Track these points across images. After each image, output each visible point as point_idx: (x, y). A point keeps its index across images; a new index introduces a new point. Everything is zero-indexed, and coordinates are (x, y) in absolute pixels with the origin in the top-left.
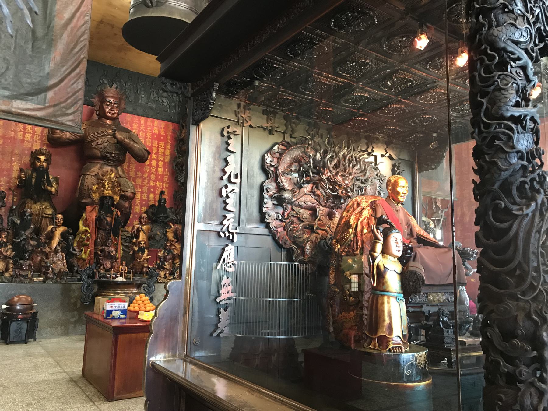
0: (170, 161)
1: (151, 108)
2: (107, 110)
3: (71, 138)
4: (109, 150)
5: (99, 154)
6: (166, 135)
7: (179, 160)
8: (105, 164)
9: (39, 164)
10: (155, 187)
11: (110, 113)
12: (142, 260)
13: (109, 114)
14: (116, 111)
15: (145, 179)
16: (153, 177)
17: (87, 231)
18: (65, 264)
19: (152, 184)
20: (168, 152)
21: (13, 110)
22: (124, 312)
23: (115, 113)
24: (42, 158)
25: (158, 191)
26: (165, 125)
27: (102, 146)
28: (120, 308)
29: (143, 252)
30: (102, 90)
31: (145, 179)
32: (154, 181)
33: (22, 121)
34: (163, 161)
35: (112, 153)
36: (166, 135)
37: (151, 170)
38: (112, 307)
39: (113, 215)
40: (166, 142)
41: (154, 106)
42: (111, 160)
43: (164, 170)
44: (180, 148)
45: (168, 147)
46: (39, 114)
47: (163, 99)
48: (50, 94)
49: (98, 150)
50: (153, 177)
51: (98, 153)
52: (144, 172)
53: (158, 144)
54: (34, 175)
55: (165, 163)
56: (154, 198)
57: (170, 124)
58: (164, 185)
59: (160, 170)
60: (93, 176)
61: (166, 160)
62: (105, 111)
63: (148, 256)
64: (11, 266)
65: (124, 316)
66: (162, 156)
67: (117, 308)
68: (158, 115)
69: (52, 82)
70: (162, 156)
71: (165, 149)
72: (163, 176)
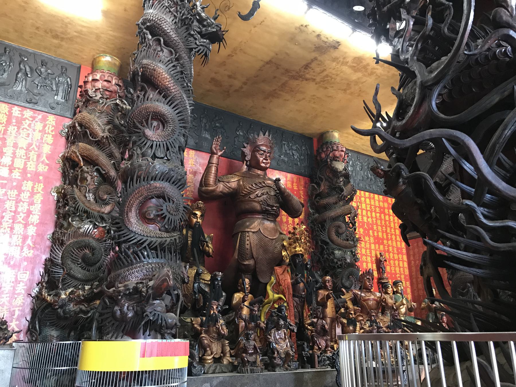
1: (283, 161)
2: (261, 159)
3: (224, 191)
6: (299, 190)
9: (195, 220)
11: (264, 163)
13: (263, 165)
14: (269, 161)
17: (280, 298)
18: (288, 344)
23: (268, 163)
24: (198, 213)
26: (297, 179)
27: (261, 198)
30: (254, 138)
35: (273, 206)
36: (299, 190)
41: (286, 159)
47: (294, 152)
51: (257, 206)
54: (190, 233)
57: (302, 178)
60: (253, 232)
62: (259, 161)
64: (228, 349)
68: (290, 168)
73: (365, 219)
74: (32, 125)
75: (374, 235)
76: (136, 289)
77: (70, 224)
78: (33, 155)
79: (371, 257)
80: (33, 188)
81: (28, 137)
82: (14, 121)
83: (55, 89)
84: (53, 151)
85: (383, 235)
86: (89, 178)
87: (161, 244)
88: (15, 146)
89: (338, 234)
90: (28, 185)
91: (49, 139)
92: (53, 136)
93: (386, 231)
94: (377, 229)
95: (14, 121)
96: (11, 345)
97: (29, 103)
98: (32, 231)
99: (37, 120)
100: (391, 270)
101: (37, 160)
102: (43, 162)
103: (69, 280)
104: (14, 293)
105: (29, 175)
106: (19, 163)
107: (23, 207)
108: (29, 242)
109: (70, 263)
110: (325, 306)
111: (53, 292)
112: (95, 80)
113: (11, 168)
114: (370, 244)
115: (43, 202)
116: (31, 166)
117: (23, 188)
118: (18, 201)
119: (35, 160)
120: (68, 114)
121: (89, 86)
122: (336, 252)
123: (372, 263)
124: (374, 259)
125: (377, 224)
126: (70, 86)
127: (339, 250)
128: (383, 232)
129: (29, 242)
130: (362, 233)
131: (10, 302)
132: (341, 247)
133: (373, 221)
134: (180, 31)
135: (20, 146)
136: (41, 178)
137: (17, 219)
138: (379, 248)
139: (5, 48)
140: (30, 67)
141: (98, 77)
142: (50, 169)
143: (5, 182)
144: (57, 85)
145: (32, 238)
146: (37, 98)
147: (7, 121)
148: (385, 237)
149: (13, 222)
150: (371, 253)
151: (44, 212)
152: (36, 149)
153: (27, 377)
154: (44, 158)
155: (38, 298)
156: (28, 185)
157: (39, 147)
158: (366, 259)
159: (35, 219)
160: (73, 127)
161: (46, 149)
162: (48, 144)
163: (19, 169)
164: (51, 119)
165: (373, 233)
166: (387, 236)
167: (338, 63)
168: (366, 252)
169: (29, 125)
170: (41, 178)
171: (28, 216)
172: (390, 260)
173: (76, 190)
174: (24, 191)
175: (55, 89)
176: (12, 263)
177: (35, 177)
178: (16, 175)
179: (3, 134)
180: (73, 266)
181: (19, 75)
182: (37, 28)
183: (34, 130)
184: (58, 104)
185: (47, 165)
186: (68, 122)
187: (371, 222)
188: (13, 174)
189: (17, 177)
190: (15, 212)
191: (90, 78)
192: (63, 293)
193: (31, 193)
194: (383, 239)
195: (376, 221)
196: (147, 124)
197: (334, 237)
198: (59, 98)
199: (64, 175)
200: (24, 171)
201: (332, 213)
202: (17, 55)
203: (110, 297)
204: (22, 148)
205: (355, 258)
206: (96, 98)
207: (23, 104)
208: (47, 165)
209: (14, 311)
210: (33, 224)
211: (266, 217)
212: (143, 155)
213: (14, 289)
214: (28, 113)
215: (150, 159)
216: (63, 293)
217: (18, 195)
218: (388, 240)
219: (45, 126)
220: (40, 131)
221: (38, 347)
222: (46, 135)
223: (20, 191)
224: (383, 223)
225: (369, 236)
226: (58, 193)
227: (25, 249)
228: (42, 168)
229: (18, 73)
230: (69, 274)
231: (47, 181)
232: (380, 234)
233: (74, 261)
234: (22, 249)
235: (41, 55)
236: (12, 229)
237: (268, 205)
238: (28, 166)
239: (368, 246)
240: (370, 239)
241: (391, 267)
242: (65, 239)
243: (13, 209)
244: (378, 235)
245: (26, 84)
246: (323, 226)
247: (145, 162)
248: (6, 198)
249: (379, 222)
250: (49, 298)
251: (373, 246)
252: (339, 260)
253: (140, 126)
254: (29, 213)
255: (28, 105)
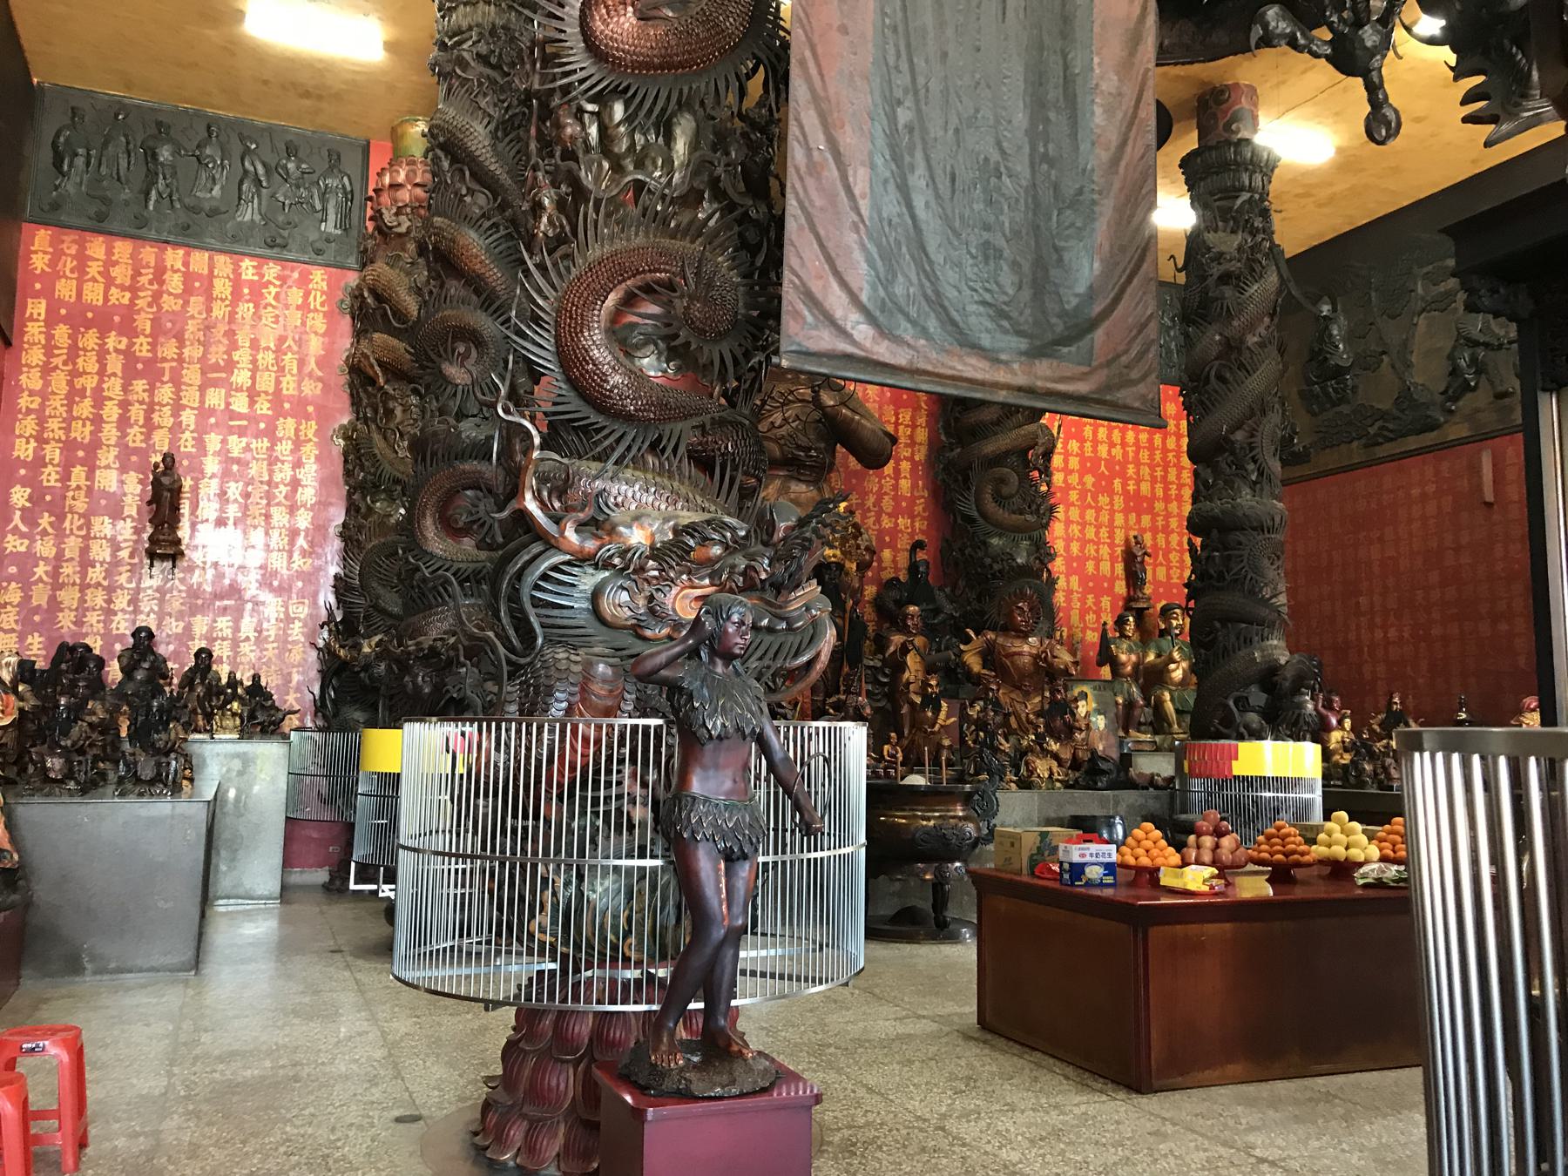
0: (928, 456)
4: (803, 441)
5: (778, 453)
7: (951, 455)
8: (792, 478)
10: (895, 531)
12: (937, 728)
15: (869, 510)
16: (887, 503)
19: (887, 523)
20: (922, 435)
21: (1039, 383)
22: (1110, 868)
25: (904, 543)
27: (783, 431)
28: (1101, 860)
29: (937, 710)
31: (869, 510)
32: (890, 515)
33: (1060, 408)
34: (911, 459)
37: (881, 487)
38: (1083, 856)
39: (844, 611)
40: (916, 409)
42: (805, 467)
43: (914, 486)
44: (957, 420)
45: (922, 421)
46: (1082, 388)
48: (1099, 334)
49: (776, 441)
50: (887, 503)
52: (867, 494)
53: (897, 414)
55: (914, 464)
56: (894, 561)
58: (917, 525)
59: (905, 484)
61: (917, 458)
63: (948, 717)
65: (1109, 880)
66: (907, 445)
67: (1094, 859)
69: (1097, 309)
70: (907, 445)
71: (914, 427)
72: (912, 501)
73: (1103, 450)
74: (283, 296)
75: (1125, 492)
76: (432, 648)
77: (370, 510)
78: (290, 360)
79: (1112, 545)
80: (297, 430)
81: (276, 322)
82: (246, 291)
83: (318, 206)
84: (329, 350)
85: (1153, 489)
86: (398, 411)
87: (476, 573)
88: (255, 345)
89: (999, 498)
90: (287, 426)
91: (319, 323)
92: (326, 315)
93: (1164, 478)
94: (1138, 473)
95: (246, 291)
96: (286, 737)
97: (272, 247)
98: (303, 520)
99: (290, 282)
100: (1169, 577)
101: (300, 369)
102: (310, 375)
103: (377, 619)
104: (286, 642)
105: (287, 406)
106: (266, 382)
107: (284, 473)
108: (301, 542)
109: (375, 585)
110: (902, 667)
111: (349, 642)
112: (395, 186)
113: (253, 395)
114: (1112, 512)
115: (318, 458)
116: (289, 386)
117: (280, 434)
118: (272, 461)
119: (295, 371)
120: (352, 261)
121: (385, 198)
122: (995, 541)
123: (1113, 560)
124: (1119, 550)
125: (1138, 464)
126: (349, 196)
127: (1000, 536)
128: (1154, 480)
129: (301, 542)
130: (1089, 486)
131: (280, 656)
132: (1003, 529)
133: (1125, 454)
134: (500, 146)
135: (263, 344)
136: (310, 409)
137: (275, 497)
138: (1139, 521)
139: (209, 127)
140: (264, 165)
141: (401, 178)
142: (326, 388)
143: (245, 423)
144: (324, 200)
145: (306, 536)
146: (285, 233)
147: (232, 293)
148: (1159, 492)
149: (268, 505)
150: (1111, 535)
151: (323, 482)
152: (295, 348)
153: (325, 791)
154: (312, 365)
155: (327, 653)
156: (287, 426)
157: (300, 343)
158: (1097, 551)
159: (308, 494)
160: (357, 295)
161: (315, 345)
162: (316, 333)
163: (266, 393)
164: (318, 276)
165: (1125, 485)
166: (1166, 489)
167: (360, 528)
168: (1097, 533)
169: (277, 297)
170: (310, 409)
171: (294, 491)
172: (1168, 551)
173: (376, 437)
174: (280, 440)
175: (318, 206)
176: (276, 583)
177: (299, 409)
178: (263, 407)
179: (229, 323)
180: (381, 591)
181: (244, 187)
182: (266, 82)
183: (287, 307)
184: (328, 241)
185: (319, 379)
186: (352, 279)
187: (1119, 457)
188: (257, 406)
189: (265, 411)
190: (269, 483)
191: (387, 180)
192: (365, 643)
193: (294, 443)
194: (1153, 499)
195: (1137, 453)
196: (445, 350)
197: (991, 506)
198: (329, 227)
199: (356, 402)
200: (277, 397)
201: (990, 447)
202: (235, 140)
203: (398, 661)
204: (268, 348)
205: (1043, 554)
206: (399, 230)
207: (259, 251)
208: (319, 379)
209: (290, 674)
210: (304, 505)
211: (795, 474)
212: (442, 411)
213: (286, 635)
214: (272, 271)
215: (452, 421)
216: (365, 643)
217: (271, 449)
218: (1167, 499)
219: (307, 294)
220: (298, 308)
221: (336, 738)
222: (311, 315)
223: (274, 440)
224: (1158, 456)
225: (1111, 493)
226: (346, 438)
227: (296, 556)
228: (311, 389)
229: (241, 183)
230: (375, 607)
231: (323, 416)
232: (1145, 488)
233: (386, 583)
234: (290, 557)
235: (284, 130)
236: (268, 516)
237: (799, 447)
238: (284, 385)
239: (1105, 518)
240: (1112, 500)
241: (1169, 568)
242: (362, 538)
243: (266, 478)
244: (1138, 490)
245: (260, 204)
246: (966, 479)
247: (443, 427)
248: (248, 456)
249: (1144, 456)
250: (342, 653)
251: (1119, 519)
252: (994, 560)
253: (433, 356)
254: (295, 484)
255: (268, 252)
